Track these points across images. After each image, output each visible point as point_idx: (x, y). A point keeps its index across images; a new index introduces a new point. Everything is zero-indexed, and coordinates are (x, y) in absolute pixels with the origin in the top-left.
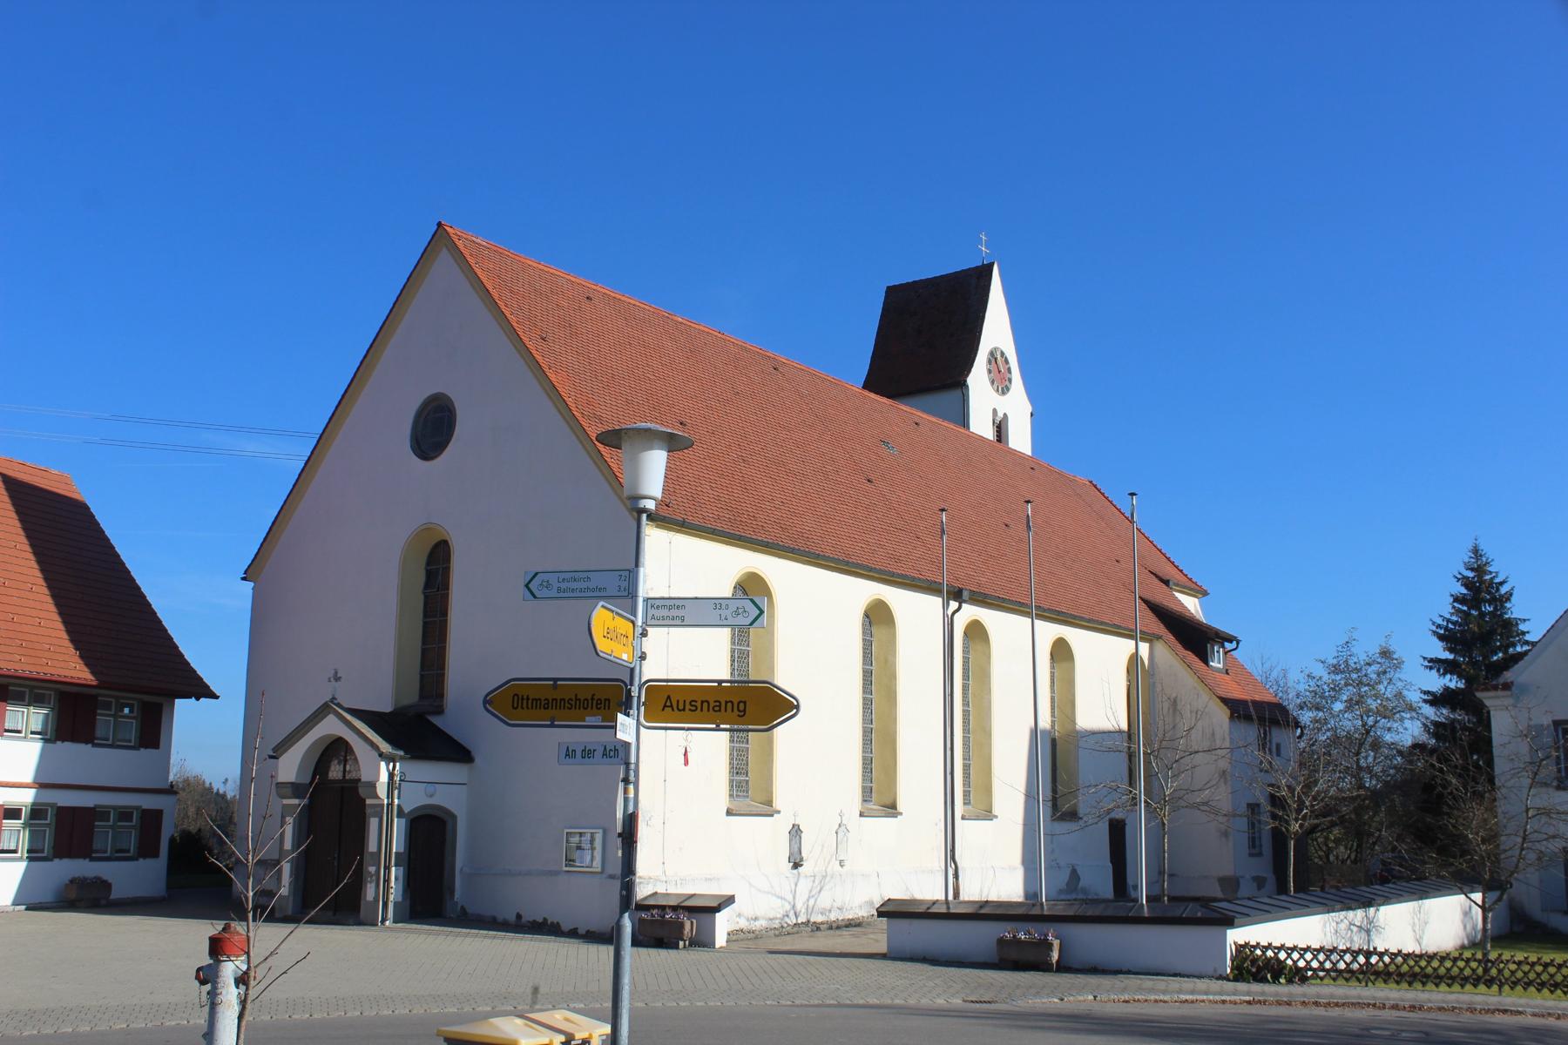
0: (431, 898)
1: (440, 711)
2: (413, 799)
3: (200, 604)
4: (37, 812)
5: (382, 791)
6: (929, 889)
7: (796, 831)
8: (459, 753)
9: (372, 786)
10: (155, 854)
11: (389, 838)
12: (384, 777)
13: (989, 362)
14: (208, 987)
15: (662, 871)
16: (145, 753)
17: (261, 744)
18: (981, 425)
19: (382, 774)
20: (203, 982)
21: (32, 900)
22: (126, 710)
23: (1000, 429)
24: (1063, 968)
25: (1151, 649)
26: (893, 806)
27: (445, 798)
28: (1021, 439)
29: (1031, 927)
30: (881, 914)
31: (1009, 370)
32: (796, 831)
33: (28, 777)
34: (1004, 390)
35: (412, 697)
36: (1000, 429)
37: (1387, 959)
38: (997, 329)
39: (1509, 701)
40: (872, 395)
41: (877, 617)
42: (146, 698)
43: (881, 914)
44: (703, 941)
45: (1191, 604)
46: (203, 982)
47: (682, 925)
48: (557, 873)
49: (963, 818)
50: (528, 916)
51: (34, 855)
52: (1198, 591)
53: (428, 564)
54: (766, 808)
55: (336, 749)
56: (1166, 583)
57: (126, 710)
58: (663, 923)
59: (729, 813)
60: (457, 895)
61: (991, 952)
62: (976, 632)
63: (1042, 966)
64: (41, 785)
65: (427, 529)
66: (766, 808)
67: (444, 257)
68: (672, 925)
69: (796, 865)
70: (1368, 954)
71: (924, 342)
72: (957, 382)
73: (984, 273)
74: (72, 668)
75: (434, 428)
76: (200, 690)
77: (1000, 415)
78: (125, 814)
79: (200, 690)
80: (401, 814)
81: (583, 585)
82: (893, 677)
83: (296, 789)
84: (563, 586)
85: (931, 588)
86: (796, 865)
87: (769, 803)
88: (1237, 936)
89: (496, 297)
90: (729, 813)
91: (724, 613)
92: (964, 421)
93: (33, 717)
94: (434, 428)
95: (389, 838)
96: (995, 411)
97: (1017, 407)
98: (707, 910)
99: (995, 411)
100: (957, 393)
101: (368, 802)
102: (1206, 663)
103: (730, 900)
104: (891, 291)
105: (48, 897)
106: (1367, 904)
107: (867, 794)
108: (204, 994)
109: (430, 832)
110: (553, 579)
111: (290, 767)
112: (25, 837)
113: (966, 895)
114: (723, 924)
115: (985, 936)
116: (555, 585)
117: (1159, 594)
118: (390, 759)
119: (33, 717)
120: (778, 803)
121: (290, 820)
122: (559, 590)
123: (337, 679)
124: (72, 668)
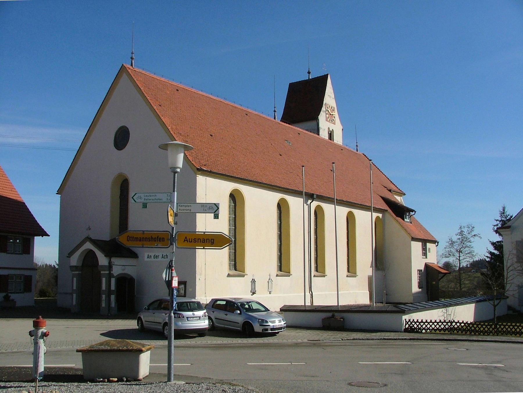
6: (298, 301)
7: (253, 281)
14: (33, 338)
16: (25, 255)
17: (65, 252)
18: (324, 134)
20: (32, 336)
22: (18, 241)
23: (331, 135)
27: (131, 271)
28: (338, 139)
32: (253, 281)
36: (331, 135)
37: (458, 324)
38: (330, 98)
39: (509, 233)
40: (283, 123)
42: (25, 236)
45: (399, 199)
46: (32, 336)
49: (177, 296)
52: (402, 194)
53: (121, 187)
56: (390, 191)
57: (18, 241)
61: (320, 324)
65: (120, 175)
67: (125, 76)
70: (451, 323)
71: (303, 102)
72: (315, 117)
75: (122, 138)
76: (44, 234)
77: (331, 130)
78: (20, 276)
79: (44, 234)
81: (153, 198)
83: (75, 268)
84: (146, 198)
88: (406, 317)
89: (143, 91)
91: (205, 208)
92: (317, 131)
94: (122, 138)
96: (329, 128)
101: (102, 272)
102: (404, 220)
104: (291, 85)
106: (445, 306)
107: (280, 269)
108: (32, 341)
110: (142, 195)
111: (75, 260)
113: (315, 304)
116: (143, 198)
117: (388, 195)
121: (75, 279)
122: (145, 199)
123: (90, 229)
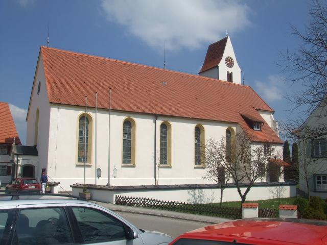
2: (26, 163)
23: (230, 76)
36: (230, 76)
96: (228, 72)
100: (215, 70)
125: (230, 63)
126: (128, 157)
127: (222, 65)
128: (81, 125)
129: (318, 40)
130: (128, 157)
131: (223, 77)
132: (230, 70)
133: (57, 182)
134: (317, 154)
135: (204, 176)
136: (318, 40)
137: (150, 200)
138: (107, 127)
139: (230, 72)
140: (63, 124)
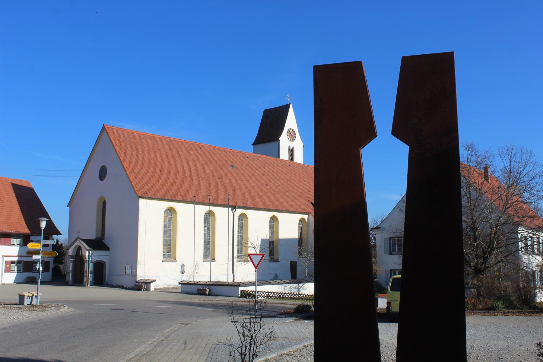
0: (100, 279)
1: (104, 239)
2: (95, 259)
3: (58, 212)
4: (19, 262)
5: (87, 257)
7: (183, 266)
8: (107, 248)
9: (85, 256)
10: (49, 271)
11: (89, 267)
12: (87, 254)
13: (288, 133)
15: (142, 275)
19: (87, 254)
21: (18, 282)
23: (291, 152)
24: (209, 295)
25: (308, 217)
26: (214, 259)
27: (102, 259)
29: (204, 286)
30: (180, 283)
31: (295, 134)
32: (183, 266)
33: (16, 254)
34: (293, 140)
35: (100, 235)
36: (291, 152)
41: (209, 216)
43: (180, 283)
44: (148, 289)
47: (142, 286)
48: (123, 275)
50: (118, 285)
51: (19, 271)
54: (175, 260)
55: (79, 248)
58: (139, 285)
59: (163, 262)
60: (106, 280)
62: (243, 216)
63: (205, 294)
64: (19, 256)
66: (175, 260)
67: (105, 133)
68: (141, 286)
69: (183, 273)
73: (288, 106)
74: (26, 230)
75: (103, 174)
80: (92, 262)
82: (214, 228)
83: (72, 257)
85: (226, 206)
86: (183, 273)
87: (175, 259)
90: (163, 262)
93: (17, 241)
94: (103, 174)
95: (89, 267)
96: (289, 147)
97: (298, 145)
98: (148, 283)
99: (289, 147)
100: (276, 143)
103: (155, 281)
104: (265, 111)
105: (22, 281)
107: (205, 256)
109: (99, 267)
112: (16, 267)
114: (153, 287)
115: (195, 289)
118: (89, 250)
119: (17, 241)
120: (178, 258)
124: (26, 230)
125: (291, 135)
126: (209, 253)
127: (284, 139)
128: (271, 226)
129: (513, 243)
130: (209, 253)
131: (284, 155)
132: (292, 144)
133: (154, 279)
134: (394, 250)
135: (246, 273)
136: (513, 243)
137: (274, 293)
138: (191, 216)
139: (291, 147)
140: (151, 213)
